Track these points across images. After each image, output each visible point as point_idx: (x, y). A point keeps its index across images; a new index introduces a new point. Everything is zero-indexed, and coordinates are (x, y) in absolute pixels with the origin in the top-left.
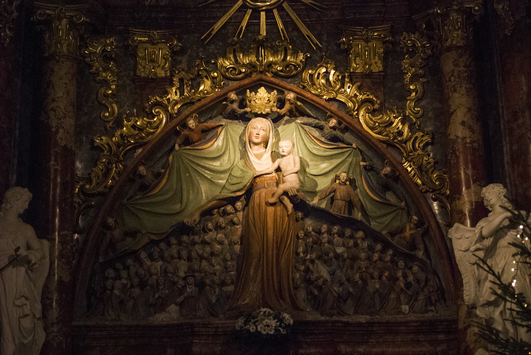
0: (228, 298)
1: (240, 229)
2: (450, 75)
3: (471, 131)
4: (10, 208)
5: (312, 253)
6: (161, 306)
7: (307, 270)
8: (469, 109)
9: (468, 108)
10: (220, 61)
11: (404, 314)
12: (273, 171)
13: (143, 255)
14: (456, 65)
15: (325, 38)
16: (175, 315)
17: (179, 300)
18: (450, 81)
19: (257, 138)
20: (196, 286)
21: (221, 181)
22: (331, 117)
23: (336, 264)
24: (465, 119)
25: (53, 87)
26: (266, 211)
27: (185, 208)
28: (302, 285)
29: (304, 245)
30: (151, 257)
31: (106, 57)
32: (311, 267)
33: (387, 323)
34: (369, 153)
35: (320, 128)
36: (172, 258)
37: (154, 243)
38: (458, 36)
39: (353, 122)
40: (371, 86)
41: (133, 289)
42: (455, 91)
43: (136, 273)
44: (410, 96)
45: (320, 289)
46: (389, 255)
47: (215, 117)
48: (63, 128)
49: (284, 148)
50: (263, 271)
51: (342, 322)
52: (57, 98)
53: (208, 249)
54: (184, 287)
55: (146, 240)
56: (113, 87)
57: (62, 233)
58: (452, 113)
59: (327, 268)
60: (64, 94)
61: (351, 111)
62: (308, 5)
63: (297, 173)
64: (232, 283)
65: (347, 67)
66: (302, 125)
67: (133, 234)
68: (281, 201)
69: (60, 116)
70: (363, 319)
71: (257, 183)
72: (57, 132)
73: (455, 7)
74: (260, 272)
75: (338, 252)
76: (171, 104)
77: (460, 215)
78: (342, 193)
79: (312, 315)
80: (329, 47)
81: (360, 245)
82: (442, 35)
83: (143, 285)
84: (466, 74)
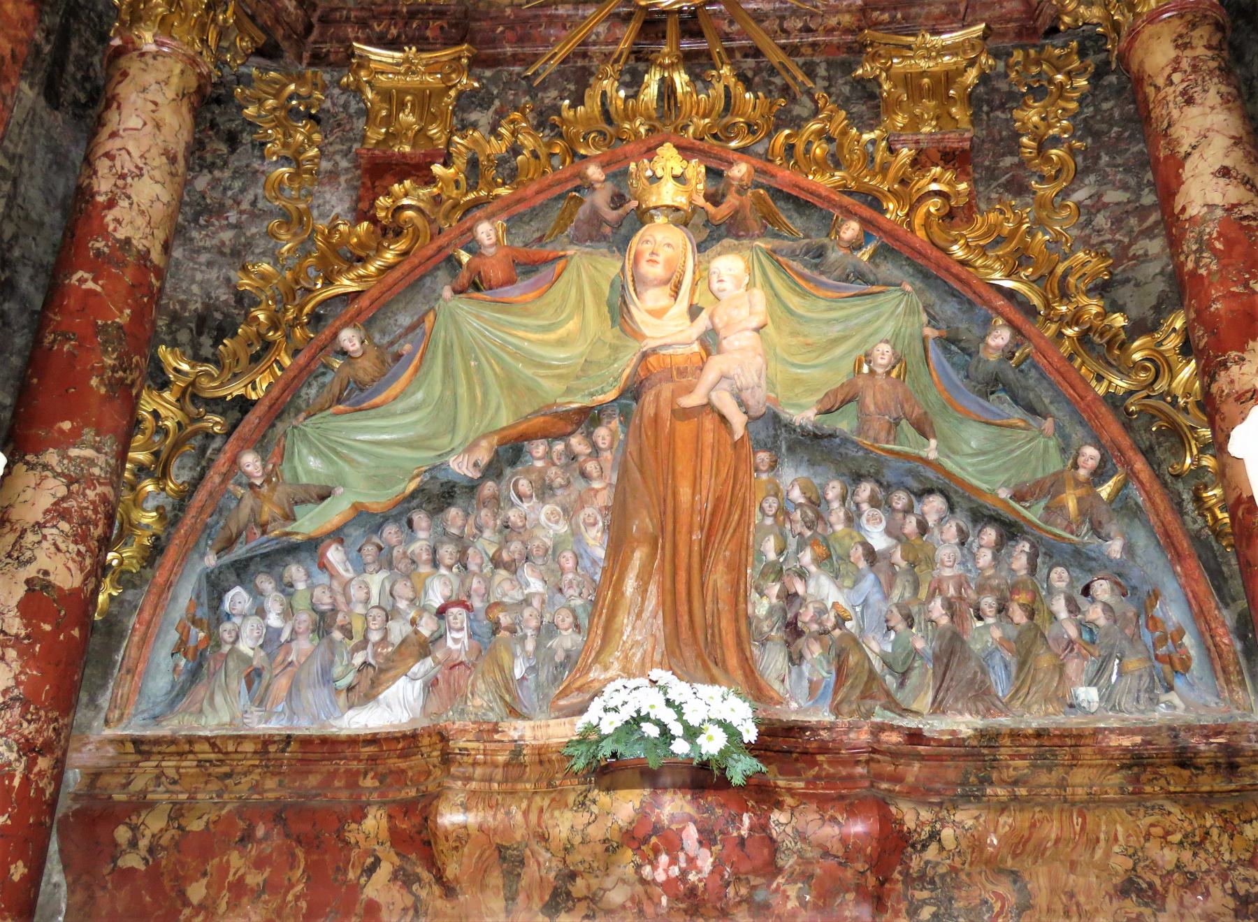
2: (1168, 70)
3: (1250, 190)
7: (789, 597)
8: (1237, 141)
9: (1233, 137)
11: (1087, 713)
18: (1171, 83)
24: (1228, 163)
26: (673, 431)
32: (799, 587)
42: (1190, 101)
48: (129, 197)
52: (125, 130)
60: (145, 124)
69: (126, 171)
70: (964, 723)
78: (879, 396)
84: (1213, 64)
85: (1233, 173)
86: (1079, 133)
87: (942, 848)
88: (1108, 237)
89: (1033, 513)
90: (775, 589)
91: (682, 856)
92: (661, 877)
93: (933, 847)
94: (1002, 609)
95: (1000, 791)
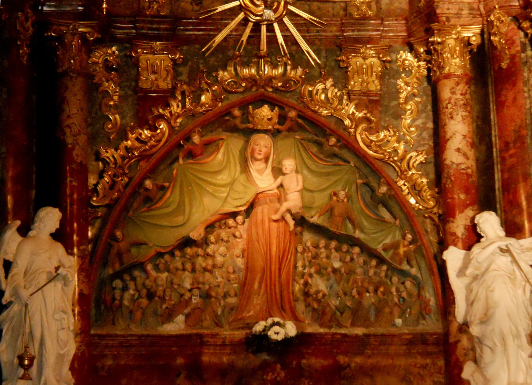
0: (232, 309)
1: (242, 243)
2: (447, 102)
3: (466, 158)
4: (44, 227)
5: (311, 267)
6: (169, 316)
7: (306, 284)
9: (464, 136)
10: (221, 73)
11: (397, 327)
12: (276, 187)
13: (149, 267)
14: (453, 93)
15: (323, 54)
16: (183, 326)
17: (186, 311)
18: (447, 108)
19: (260, 154)
20: (200, 297)
21: (222, 195)
22: (330, 135)
23: (334, 279)
24: (460, 146)
25: (68, 104)
27: (188, 220)
28: (302, 298)
29: (302, 259)
30: (157, 268)
31: (108, 67)
32: (310, 281)
33: (383, 335)
34: (366, 171)
35: (320, 145)
36: (177, 269)
37: (160, 255)
38: (456, 65)
39: (351, 140)
40: (368, 104)
41: (140, 300)
42: (452, 118)
43: (144, 285)
44: (405, 115)
45: (318, 301)
46: (384, 270)
47: (215, 130)
49: (288, 167)
50: (266, 285)
51: (340, 334)
52: (73, 114)
53: (210, 262)
54: (190, 298)
55: (152, 252)
56: (116, 98)
57: (82, 248)
58: (449, 139)
59: (325, 282)
60: (78, 111)
61: (348, 128)
62: (308, 20)
63: (299, 191)
64: (236, 295)
65: (346, 84)
66: (301, 141)
67: (139, 244)
68: (283, 218)
70: (359, 331)
71: (259, 199)
72: (73, 149)
73: (454, 36)
74: (263, 286)
75: (336, 267)
76: (174, 117)
77: (453, 238)
79: (312, 328)
80: (328, 63)
81: (356, 260)
82: (441, 62)
83: (151, 296)
84: (462, 102)
85: (461, 151)
86: (421, 94)
87: (351, 369)
88: (426, 142)
89: (387, 256)
90: (302, 281)
91: (276, 373)
92: (269, 378)
93: (348, 369)
94: (376, 291)
95: (369, 352)
